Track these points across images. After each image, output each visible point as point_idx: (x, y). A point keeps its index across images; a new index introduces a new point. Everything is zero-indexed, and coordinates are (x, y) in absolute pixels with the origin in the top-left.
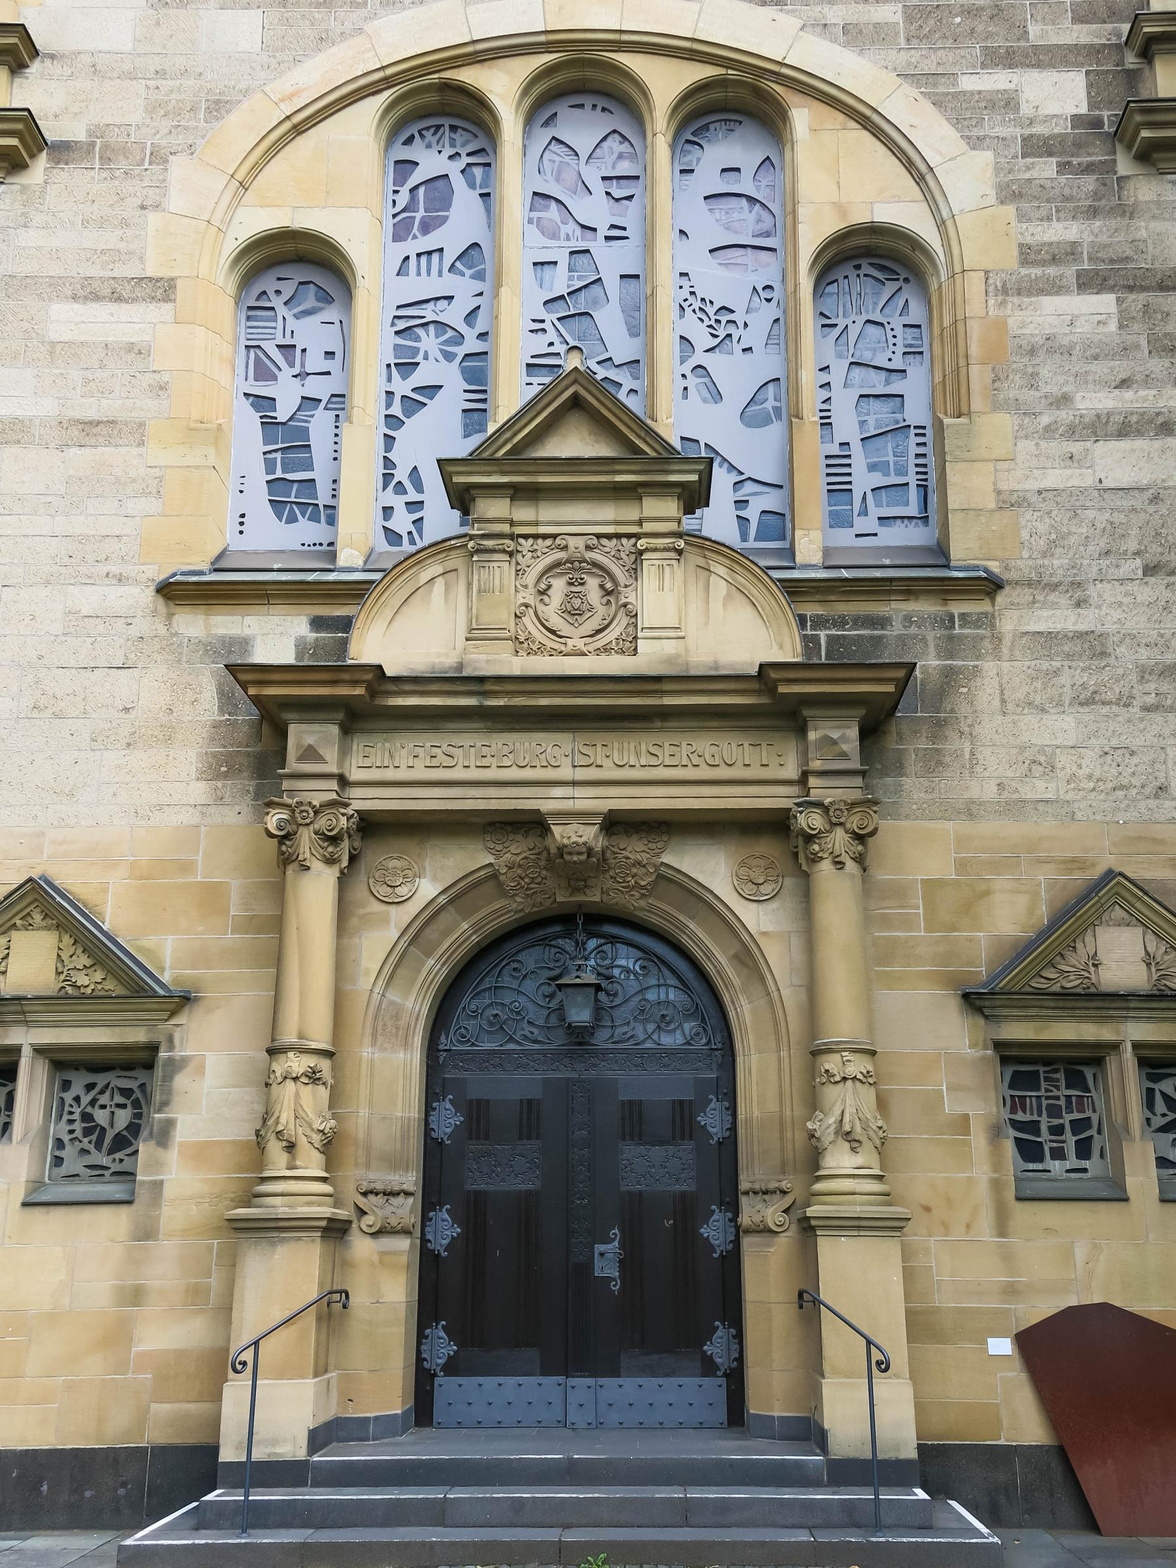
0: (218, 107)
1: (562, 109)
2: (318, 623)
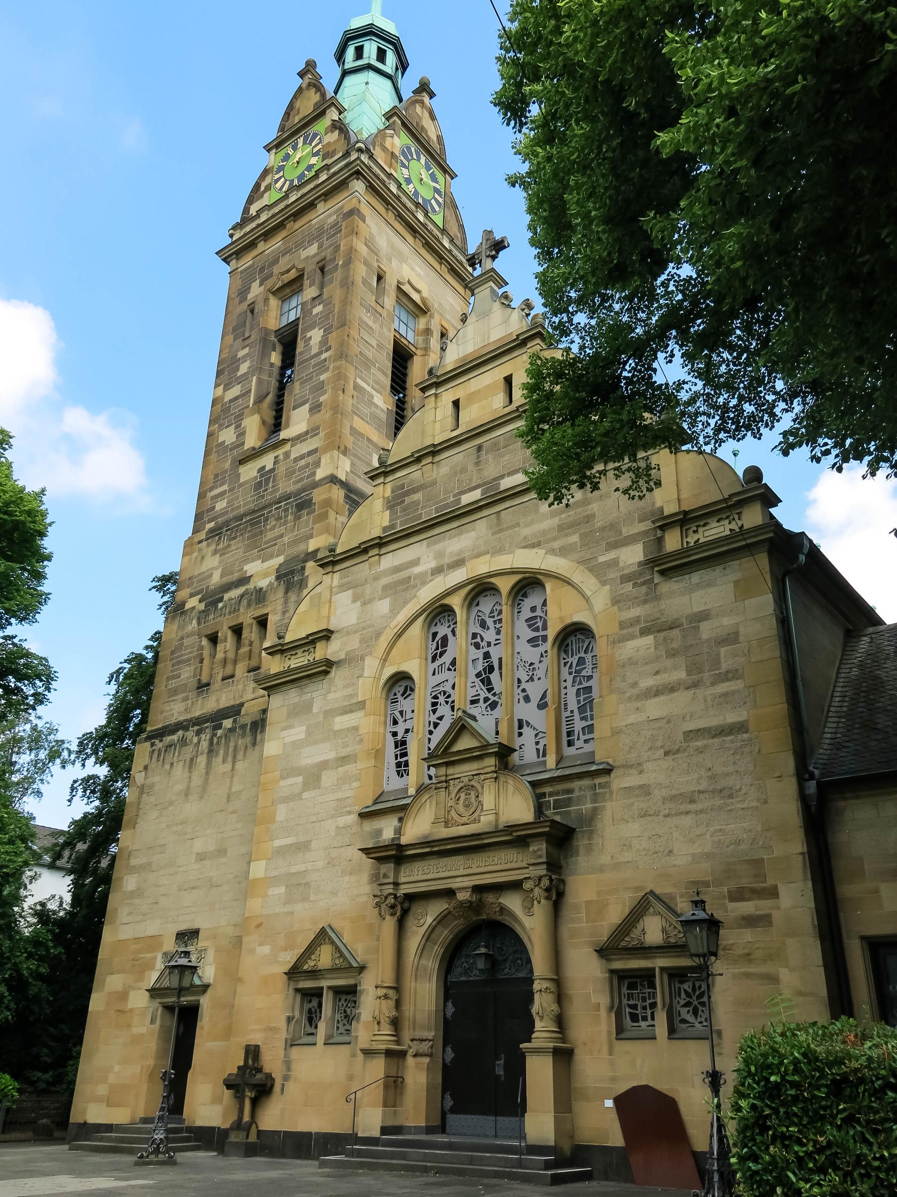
0: (378, 635)
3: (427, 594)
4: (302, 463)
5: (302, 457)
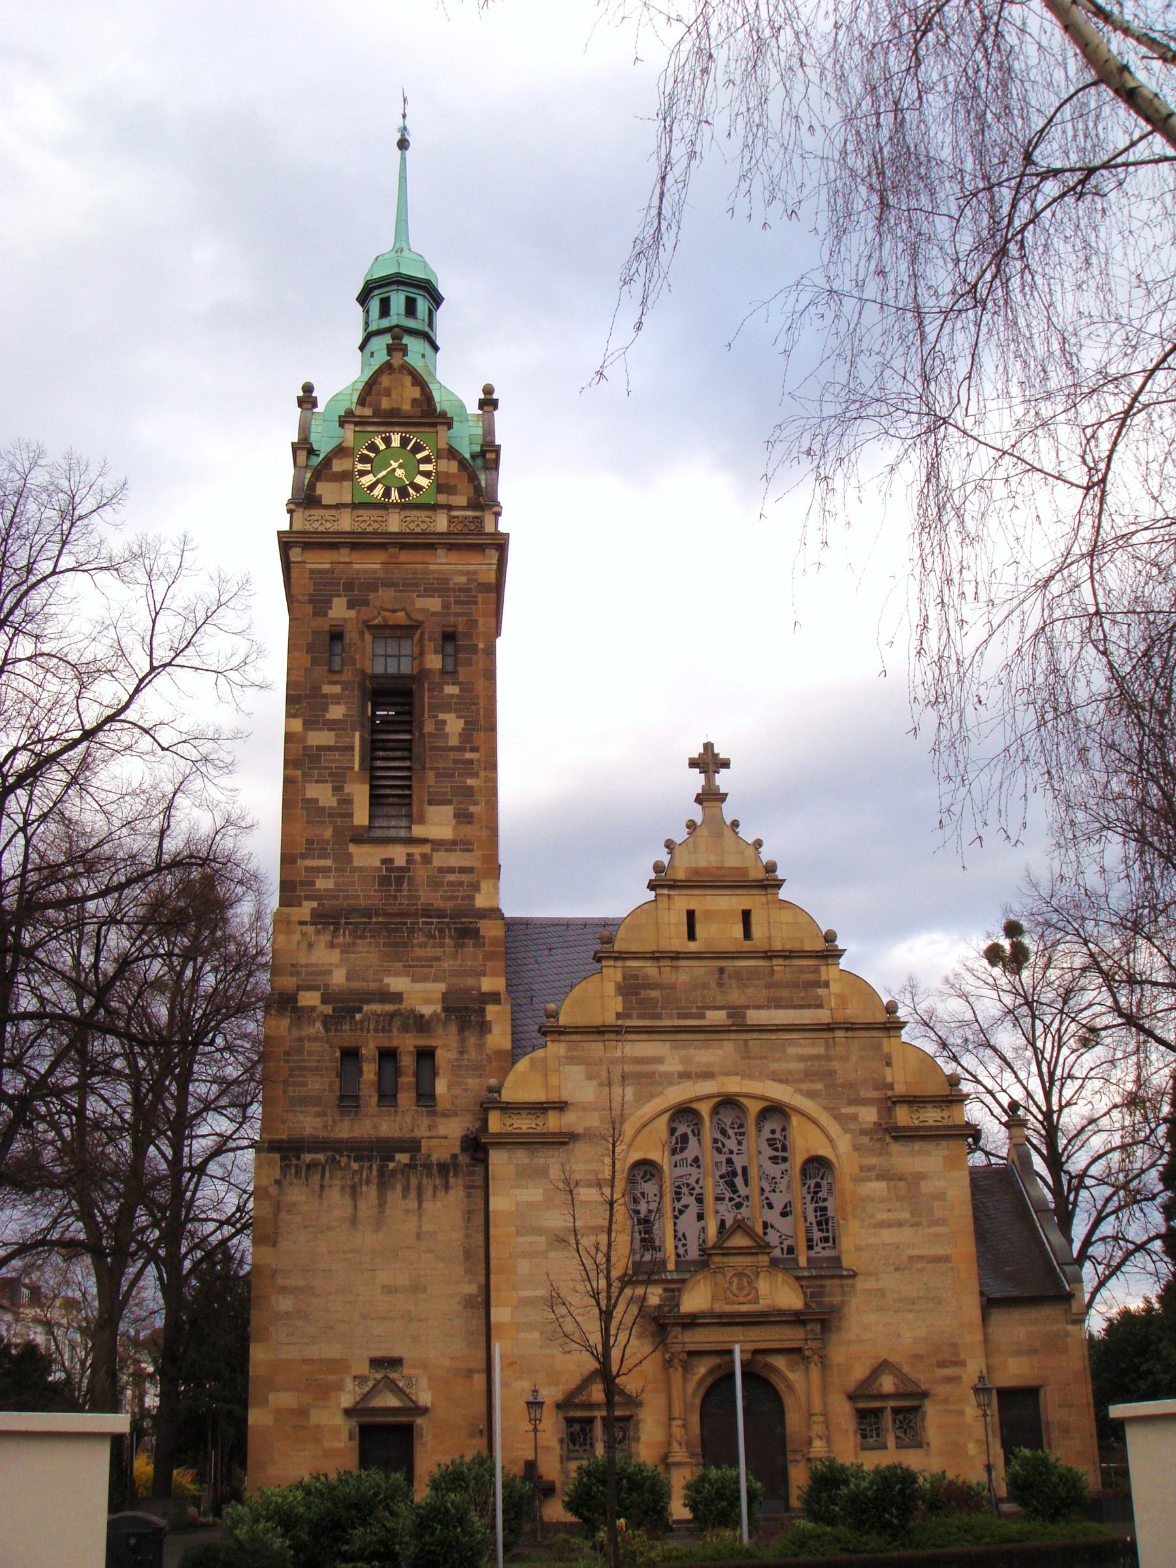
1: (722, 1110)
2: (665, 1290)
3: (677, 1094)
4: (451, 877)
5: (451, 870)
